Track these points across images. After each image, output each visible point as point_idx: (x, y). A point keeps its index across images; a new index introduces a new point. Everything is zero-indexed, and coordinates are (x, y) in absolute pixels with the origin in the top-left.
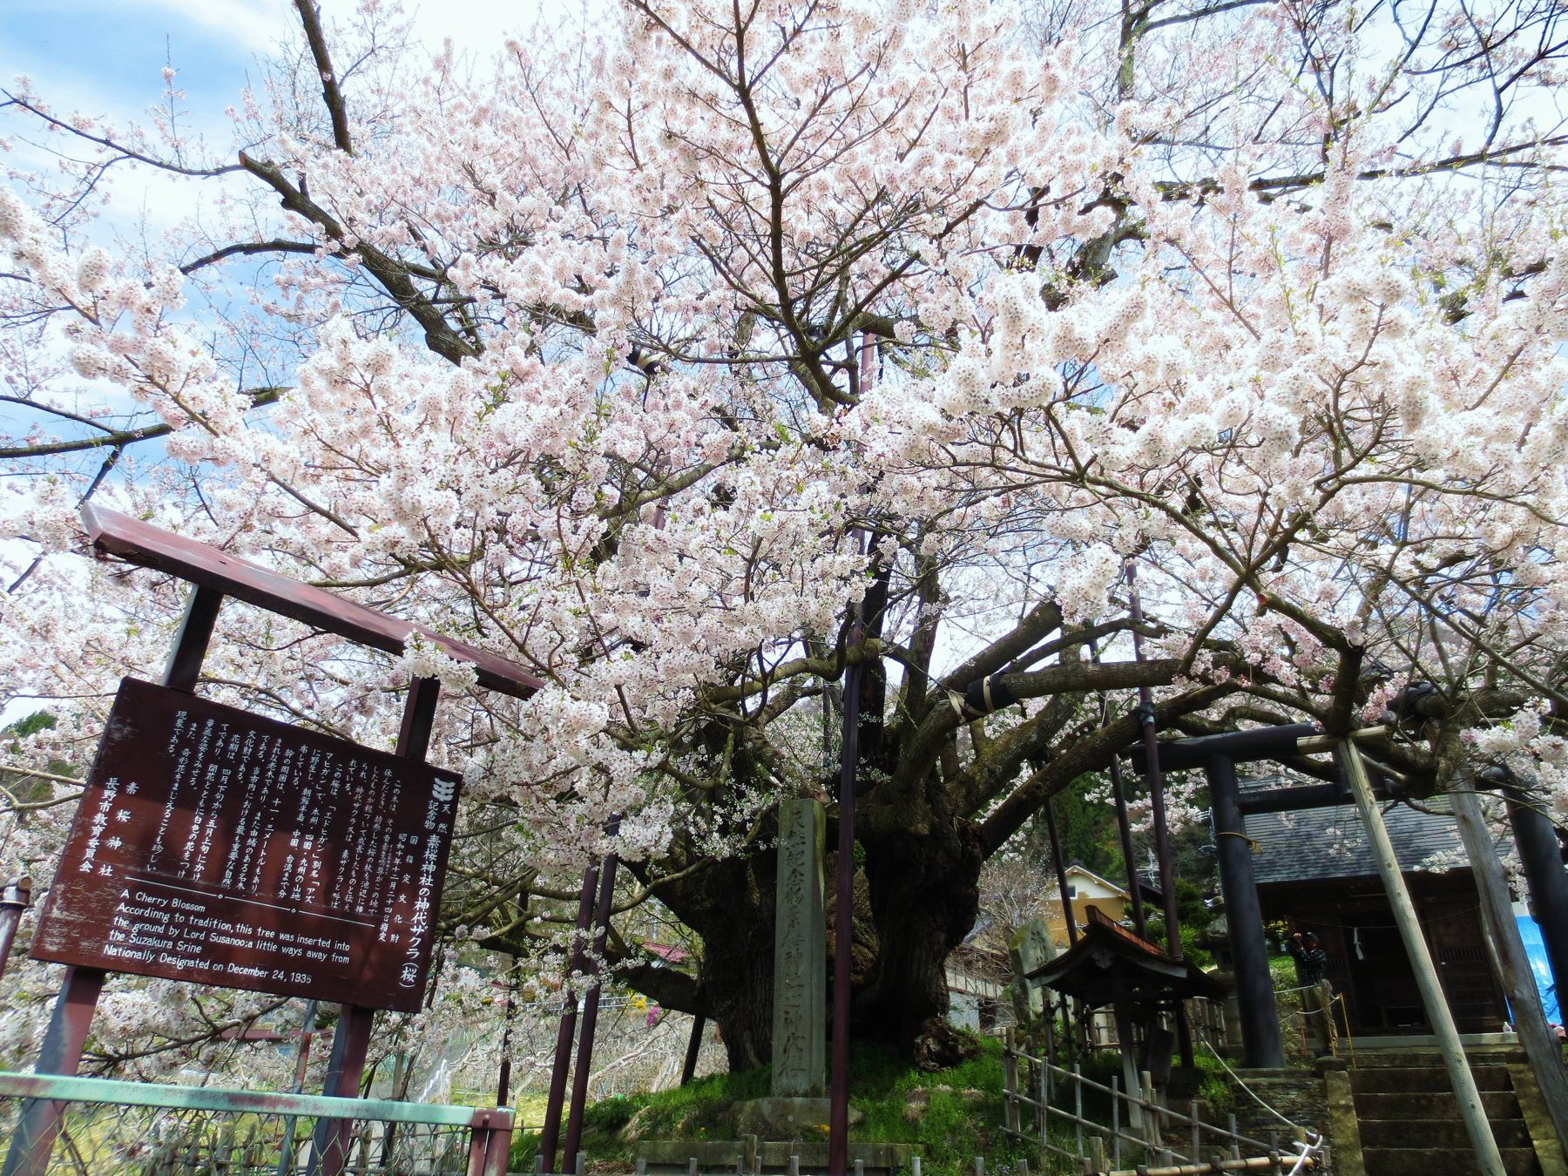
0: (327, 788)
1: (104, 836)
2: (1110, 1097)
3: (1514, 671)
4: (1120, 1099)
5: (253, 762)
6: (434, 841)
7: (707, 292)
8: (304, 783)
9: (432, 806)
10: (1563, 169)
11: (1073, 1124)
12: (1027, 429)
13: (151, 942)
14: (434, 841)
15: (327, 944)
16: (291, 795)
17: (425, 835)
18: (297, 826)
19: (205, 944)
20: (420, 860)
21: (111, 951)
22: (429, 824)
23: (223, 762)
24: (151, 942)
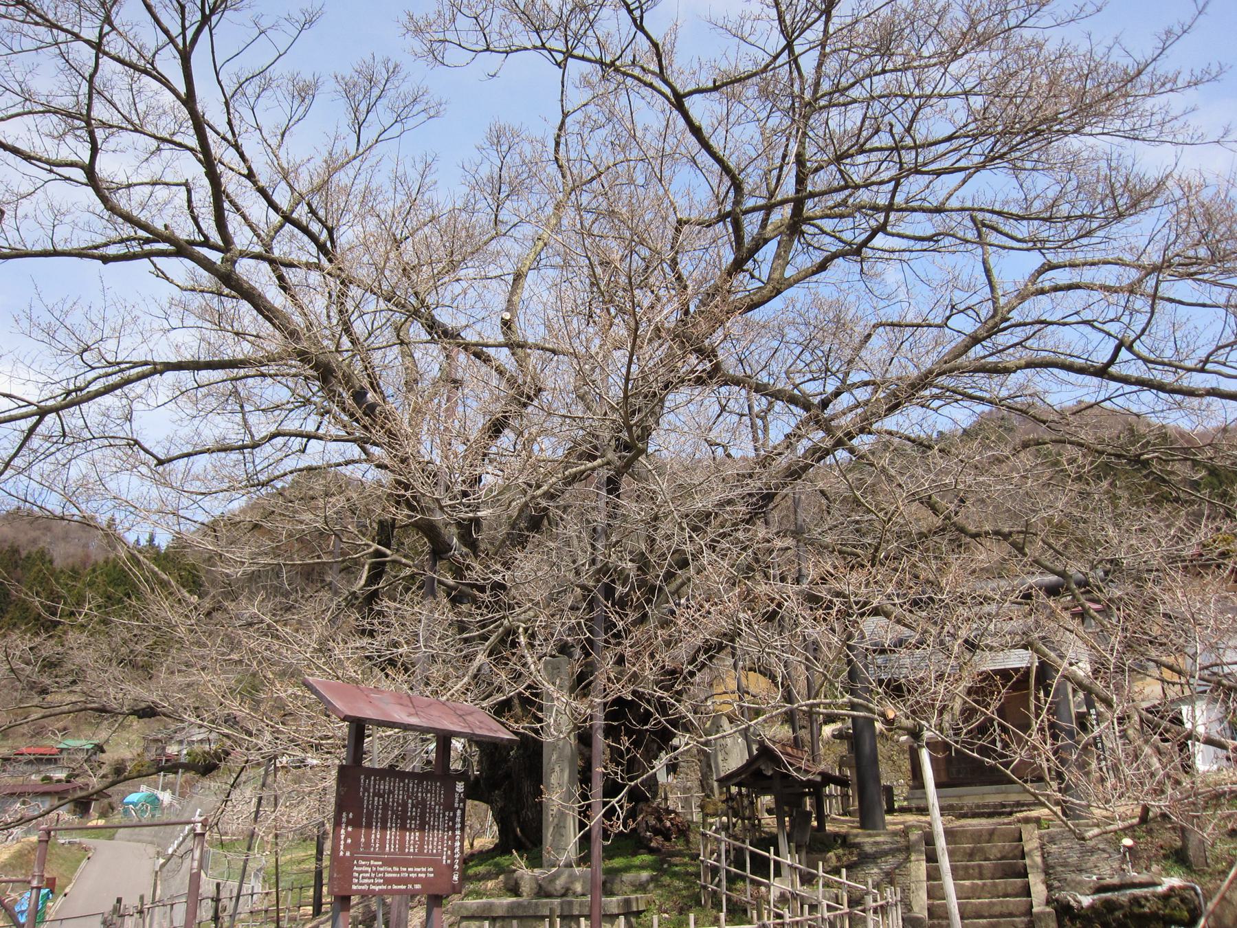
0: (417, 797)
1: (345, 840)
2: (768, 859)
3: (896, 690)
4: (775, 861)
5: (390, 792)
6: (459, 812)
7: (32, 686)
8: (409, 797)
9: (457, 796)
10: (2, 120)
11: (743, 878)
12: (971, 289)
13: (366, 881)
14: (459, 812)
15: (424, 869)
16: (405, 804)
17: (455, 810)
18: (408, 818)
19: (383, 878)
20: (454, 823)
21: (354, 887)
22: (456, 805)
23: (380, 796)
24: (366, 881)
